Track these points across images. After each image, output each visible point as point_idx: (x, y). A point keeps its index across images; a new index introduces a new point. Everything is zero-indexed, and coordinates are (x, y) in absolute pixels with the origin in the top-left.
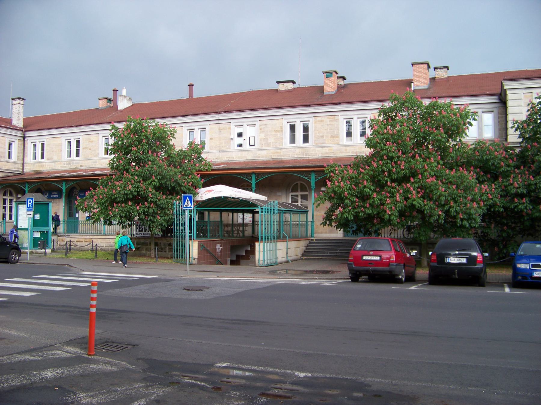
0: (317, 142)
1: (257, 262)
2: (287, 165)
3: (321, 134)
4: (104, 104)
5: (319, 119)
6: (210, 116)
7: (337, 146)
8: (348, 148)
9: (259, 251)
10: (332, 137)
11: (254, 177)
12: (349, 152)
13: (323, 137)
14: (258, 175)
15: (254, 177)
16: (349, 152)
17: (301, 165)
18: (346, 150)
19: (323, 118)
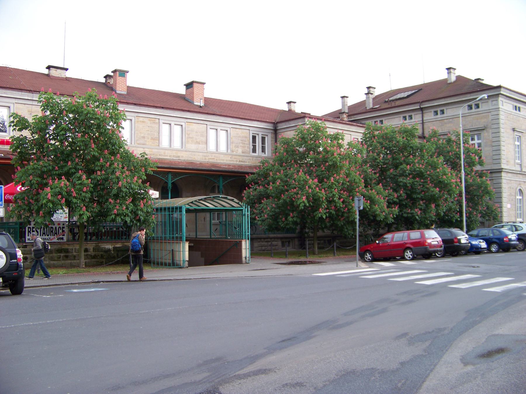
0: (138, 142)
1: (244, 259)
2: (163, 166)
3: (142, 135)
4: (182, 91)
5: (141, 119)
6: (20, 93)
7: (157, 149)
8: (167, 152)
9: (246, 249)
10: (152, 139)
11: (170, 176)
12: (167, 156)
13: (144, 137)
14: (175, 174)
15: (170, 176)
16: (167, 156)
17: (190, 167)
18: (165, 153)
19: (146, 120)
